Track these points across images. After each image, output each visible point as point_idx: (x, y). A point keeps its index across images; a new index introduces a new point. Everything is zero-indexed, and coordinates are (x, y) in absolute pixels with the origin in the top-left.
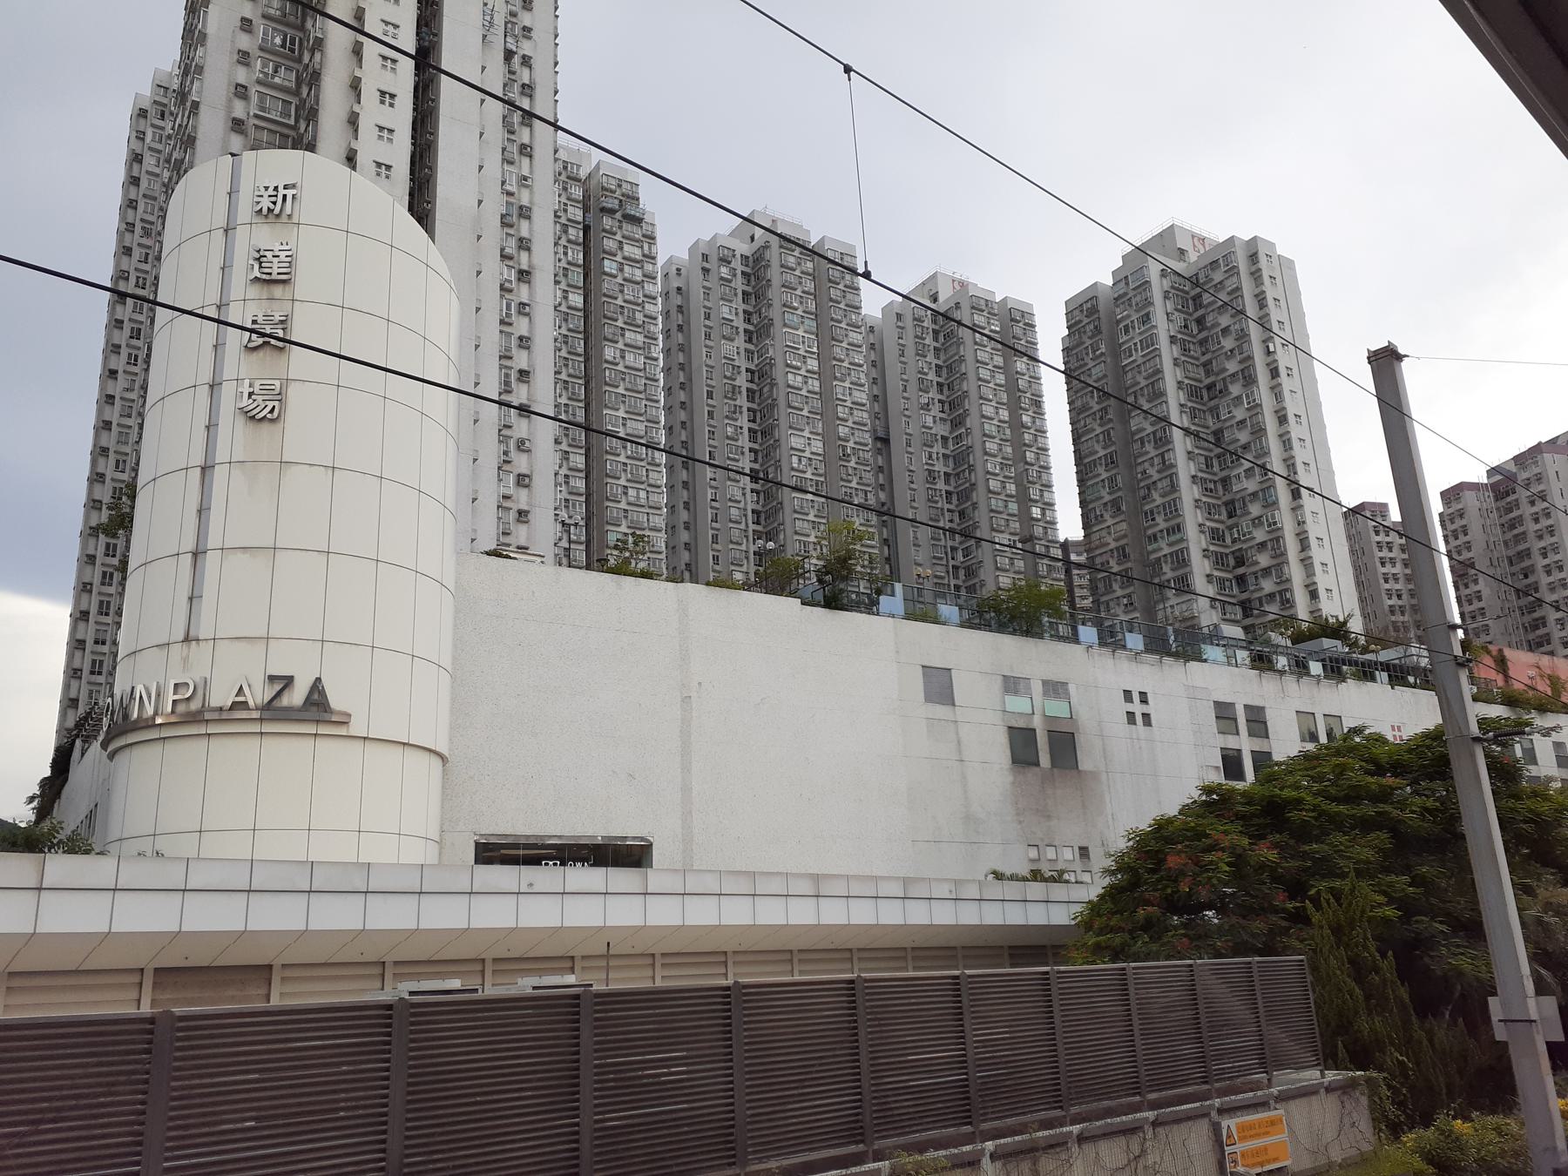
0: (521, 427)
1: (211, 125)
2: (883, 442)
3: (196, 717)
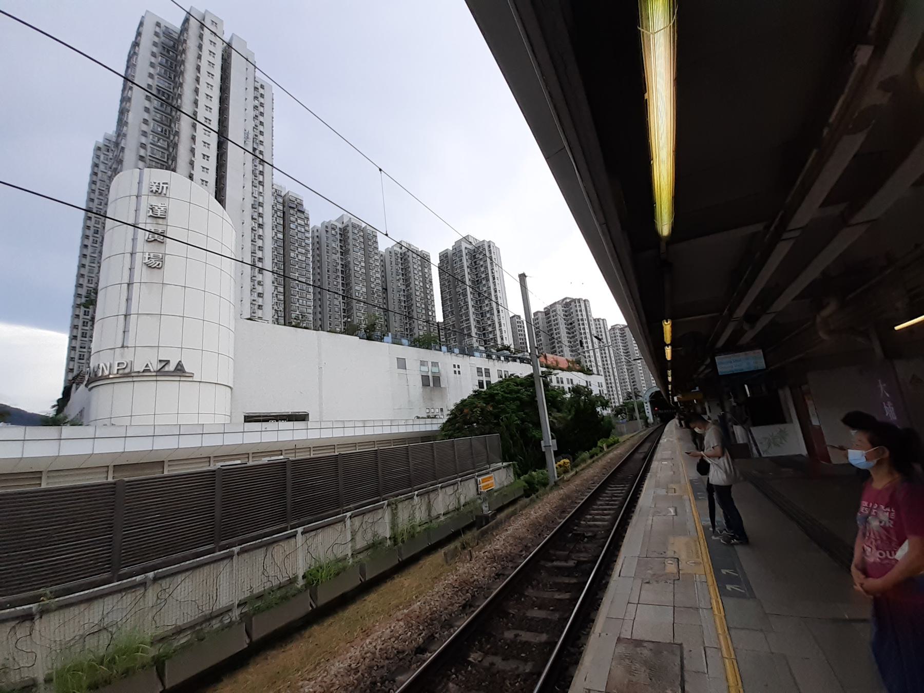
0: (259, 277)
1: (129, 156)
2: (385, 290)
3: (127, 375)
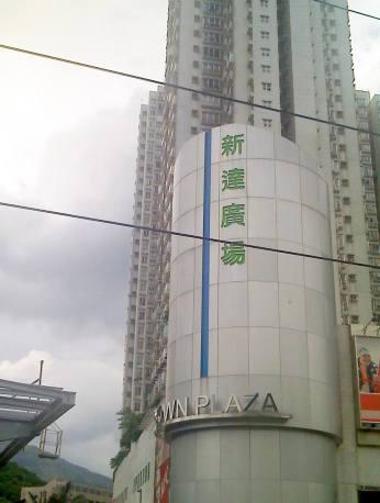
0: (351, 269)
